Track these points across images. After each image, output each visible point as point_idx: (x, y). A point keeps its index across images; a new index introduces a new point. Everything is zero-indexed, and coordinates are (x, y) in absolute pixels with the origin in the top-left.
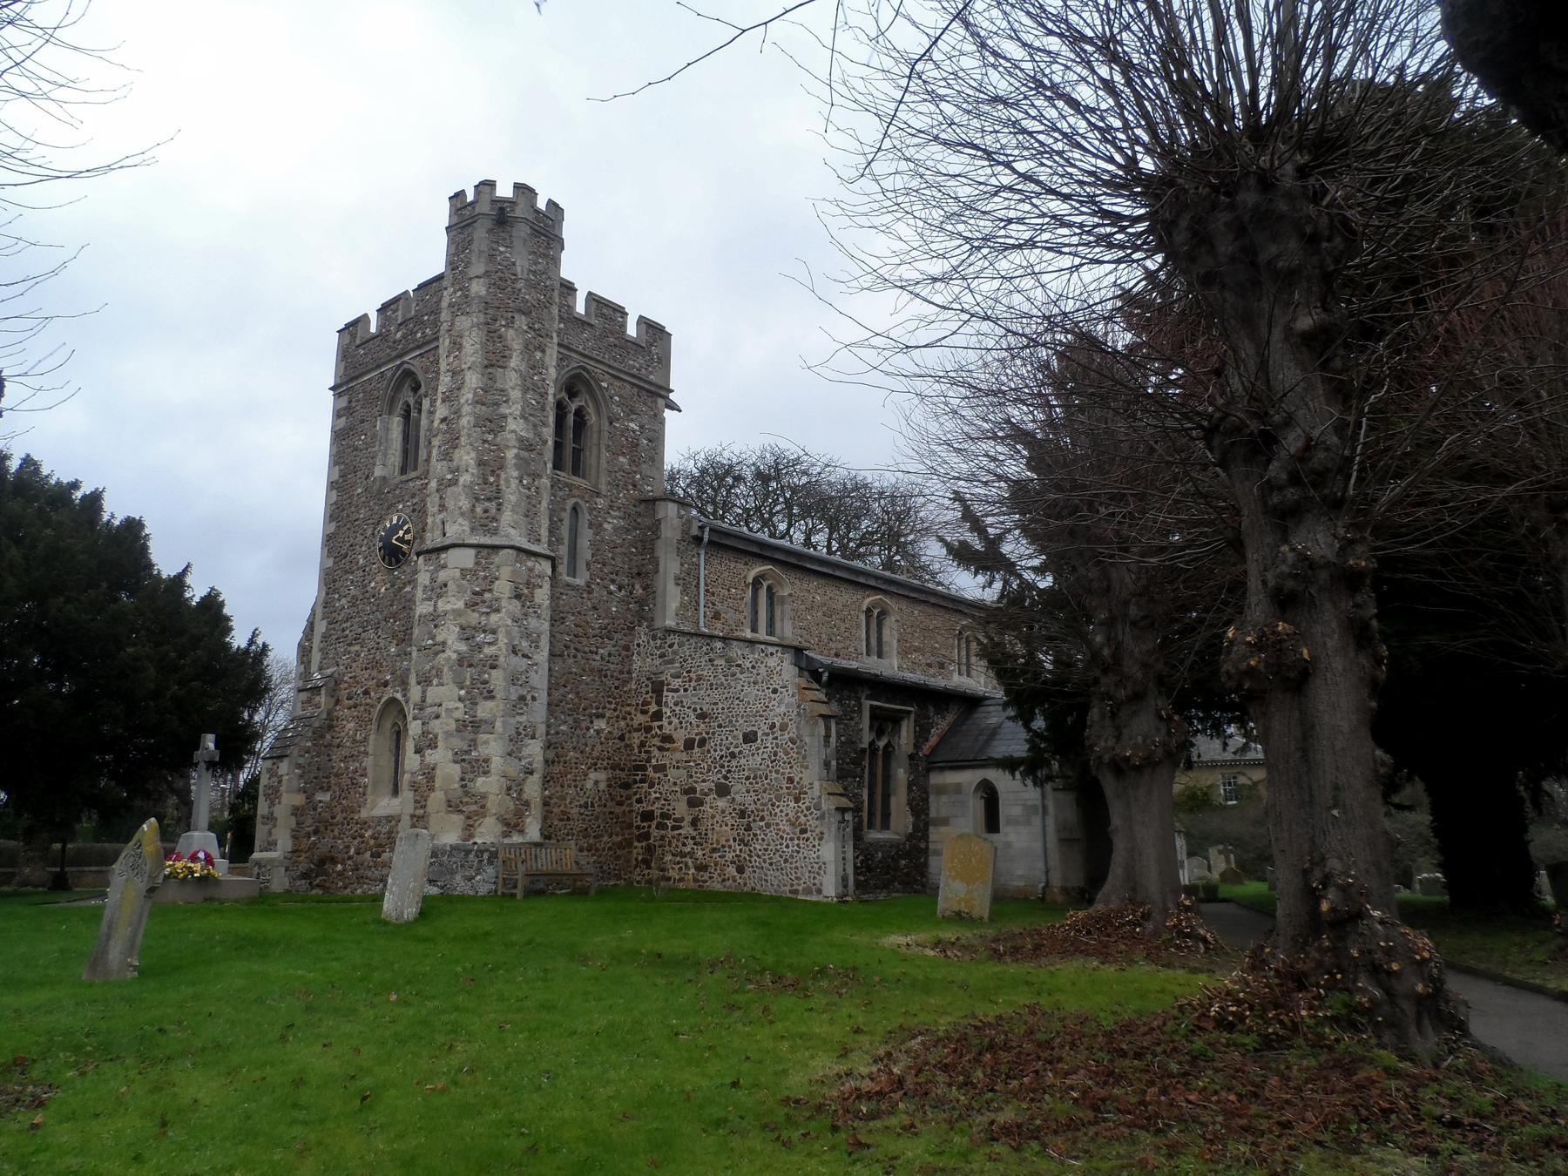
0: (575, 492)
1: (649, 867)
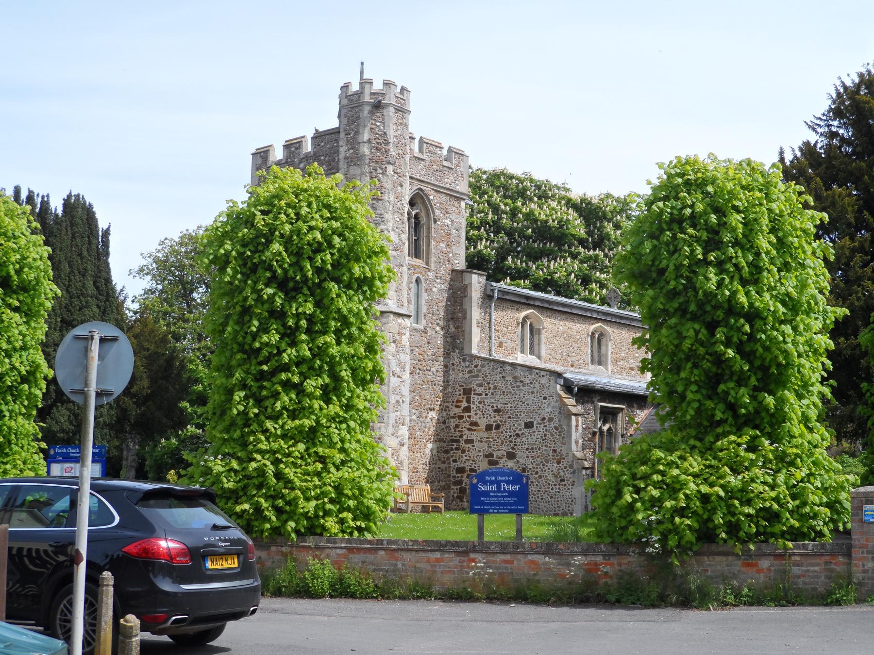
0: (418, 270)
1: (462, 501)
